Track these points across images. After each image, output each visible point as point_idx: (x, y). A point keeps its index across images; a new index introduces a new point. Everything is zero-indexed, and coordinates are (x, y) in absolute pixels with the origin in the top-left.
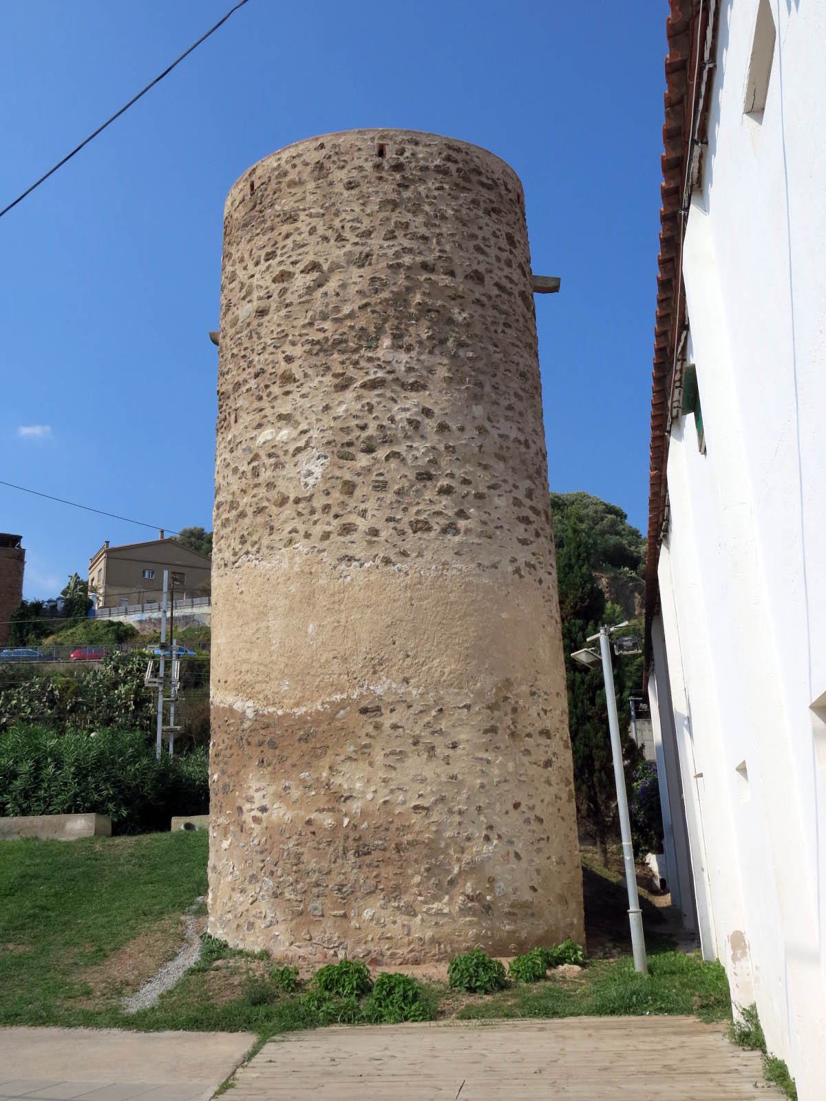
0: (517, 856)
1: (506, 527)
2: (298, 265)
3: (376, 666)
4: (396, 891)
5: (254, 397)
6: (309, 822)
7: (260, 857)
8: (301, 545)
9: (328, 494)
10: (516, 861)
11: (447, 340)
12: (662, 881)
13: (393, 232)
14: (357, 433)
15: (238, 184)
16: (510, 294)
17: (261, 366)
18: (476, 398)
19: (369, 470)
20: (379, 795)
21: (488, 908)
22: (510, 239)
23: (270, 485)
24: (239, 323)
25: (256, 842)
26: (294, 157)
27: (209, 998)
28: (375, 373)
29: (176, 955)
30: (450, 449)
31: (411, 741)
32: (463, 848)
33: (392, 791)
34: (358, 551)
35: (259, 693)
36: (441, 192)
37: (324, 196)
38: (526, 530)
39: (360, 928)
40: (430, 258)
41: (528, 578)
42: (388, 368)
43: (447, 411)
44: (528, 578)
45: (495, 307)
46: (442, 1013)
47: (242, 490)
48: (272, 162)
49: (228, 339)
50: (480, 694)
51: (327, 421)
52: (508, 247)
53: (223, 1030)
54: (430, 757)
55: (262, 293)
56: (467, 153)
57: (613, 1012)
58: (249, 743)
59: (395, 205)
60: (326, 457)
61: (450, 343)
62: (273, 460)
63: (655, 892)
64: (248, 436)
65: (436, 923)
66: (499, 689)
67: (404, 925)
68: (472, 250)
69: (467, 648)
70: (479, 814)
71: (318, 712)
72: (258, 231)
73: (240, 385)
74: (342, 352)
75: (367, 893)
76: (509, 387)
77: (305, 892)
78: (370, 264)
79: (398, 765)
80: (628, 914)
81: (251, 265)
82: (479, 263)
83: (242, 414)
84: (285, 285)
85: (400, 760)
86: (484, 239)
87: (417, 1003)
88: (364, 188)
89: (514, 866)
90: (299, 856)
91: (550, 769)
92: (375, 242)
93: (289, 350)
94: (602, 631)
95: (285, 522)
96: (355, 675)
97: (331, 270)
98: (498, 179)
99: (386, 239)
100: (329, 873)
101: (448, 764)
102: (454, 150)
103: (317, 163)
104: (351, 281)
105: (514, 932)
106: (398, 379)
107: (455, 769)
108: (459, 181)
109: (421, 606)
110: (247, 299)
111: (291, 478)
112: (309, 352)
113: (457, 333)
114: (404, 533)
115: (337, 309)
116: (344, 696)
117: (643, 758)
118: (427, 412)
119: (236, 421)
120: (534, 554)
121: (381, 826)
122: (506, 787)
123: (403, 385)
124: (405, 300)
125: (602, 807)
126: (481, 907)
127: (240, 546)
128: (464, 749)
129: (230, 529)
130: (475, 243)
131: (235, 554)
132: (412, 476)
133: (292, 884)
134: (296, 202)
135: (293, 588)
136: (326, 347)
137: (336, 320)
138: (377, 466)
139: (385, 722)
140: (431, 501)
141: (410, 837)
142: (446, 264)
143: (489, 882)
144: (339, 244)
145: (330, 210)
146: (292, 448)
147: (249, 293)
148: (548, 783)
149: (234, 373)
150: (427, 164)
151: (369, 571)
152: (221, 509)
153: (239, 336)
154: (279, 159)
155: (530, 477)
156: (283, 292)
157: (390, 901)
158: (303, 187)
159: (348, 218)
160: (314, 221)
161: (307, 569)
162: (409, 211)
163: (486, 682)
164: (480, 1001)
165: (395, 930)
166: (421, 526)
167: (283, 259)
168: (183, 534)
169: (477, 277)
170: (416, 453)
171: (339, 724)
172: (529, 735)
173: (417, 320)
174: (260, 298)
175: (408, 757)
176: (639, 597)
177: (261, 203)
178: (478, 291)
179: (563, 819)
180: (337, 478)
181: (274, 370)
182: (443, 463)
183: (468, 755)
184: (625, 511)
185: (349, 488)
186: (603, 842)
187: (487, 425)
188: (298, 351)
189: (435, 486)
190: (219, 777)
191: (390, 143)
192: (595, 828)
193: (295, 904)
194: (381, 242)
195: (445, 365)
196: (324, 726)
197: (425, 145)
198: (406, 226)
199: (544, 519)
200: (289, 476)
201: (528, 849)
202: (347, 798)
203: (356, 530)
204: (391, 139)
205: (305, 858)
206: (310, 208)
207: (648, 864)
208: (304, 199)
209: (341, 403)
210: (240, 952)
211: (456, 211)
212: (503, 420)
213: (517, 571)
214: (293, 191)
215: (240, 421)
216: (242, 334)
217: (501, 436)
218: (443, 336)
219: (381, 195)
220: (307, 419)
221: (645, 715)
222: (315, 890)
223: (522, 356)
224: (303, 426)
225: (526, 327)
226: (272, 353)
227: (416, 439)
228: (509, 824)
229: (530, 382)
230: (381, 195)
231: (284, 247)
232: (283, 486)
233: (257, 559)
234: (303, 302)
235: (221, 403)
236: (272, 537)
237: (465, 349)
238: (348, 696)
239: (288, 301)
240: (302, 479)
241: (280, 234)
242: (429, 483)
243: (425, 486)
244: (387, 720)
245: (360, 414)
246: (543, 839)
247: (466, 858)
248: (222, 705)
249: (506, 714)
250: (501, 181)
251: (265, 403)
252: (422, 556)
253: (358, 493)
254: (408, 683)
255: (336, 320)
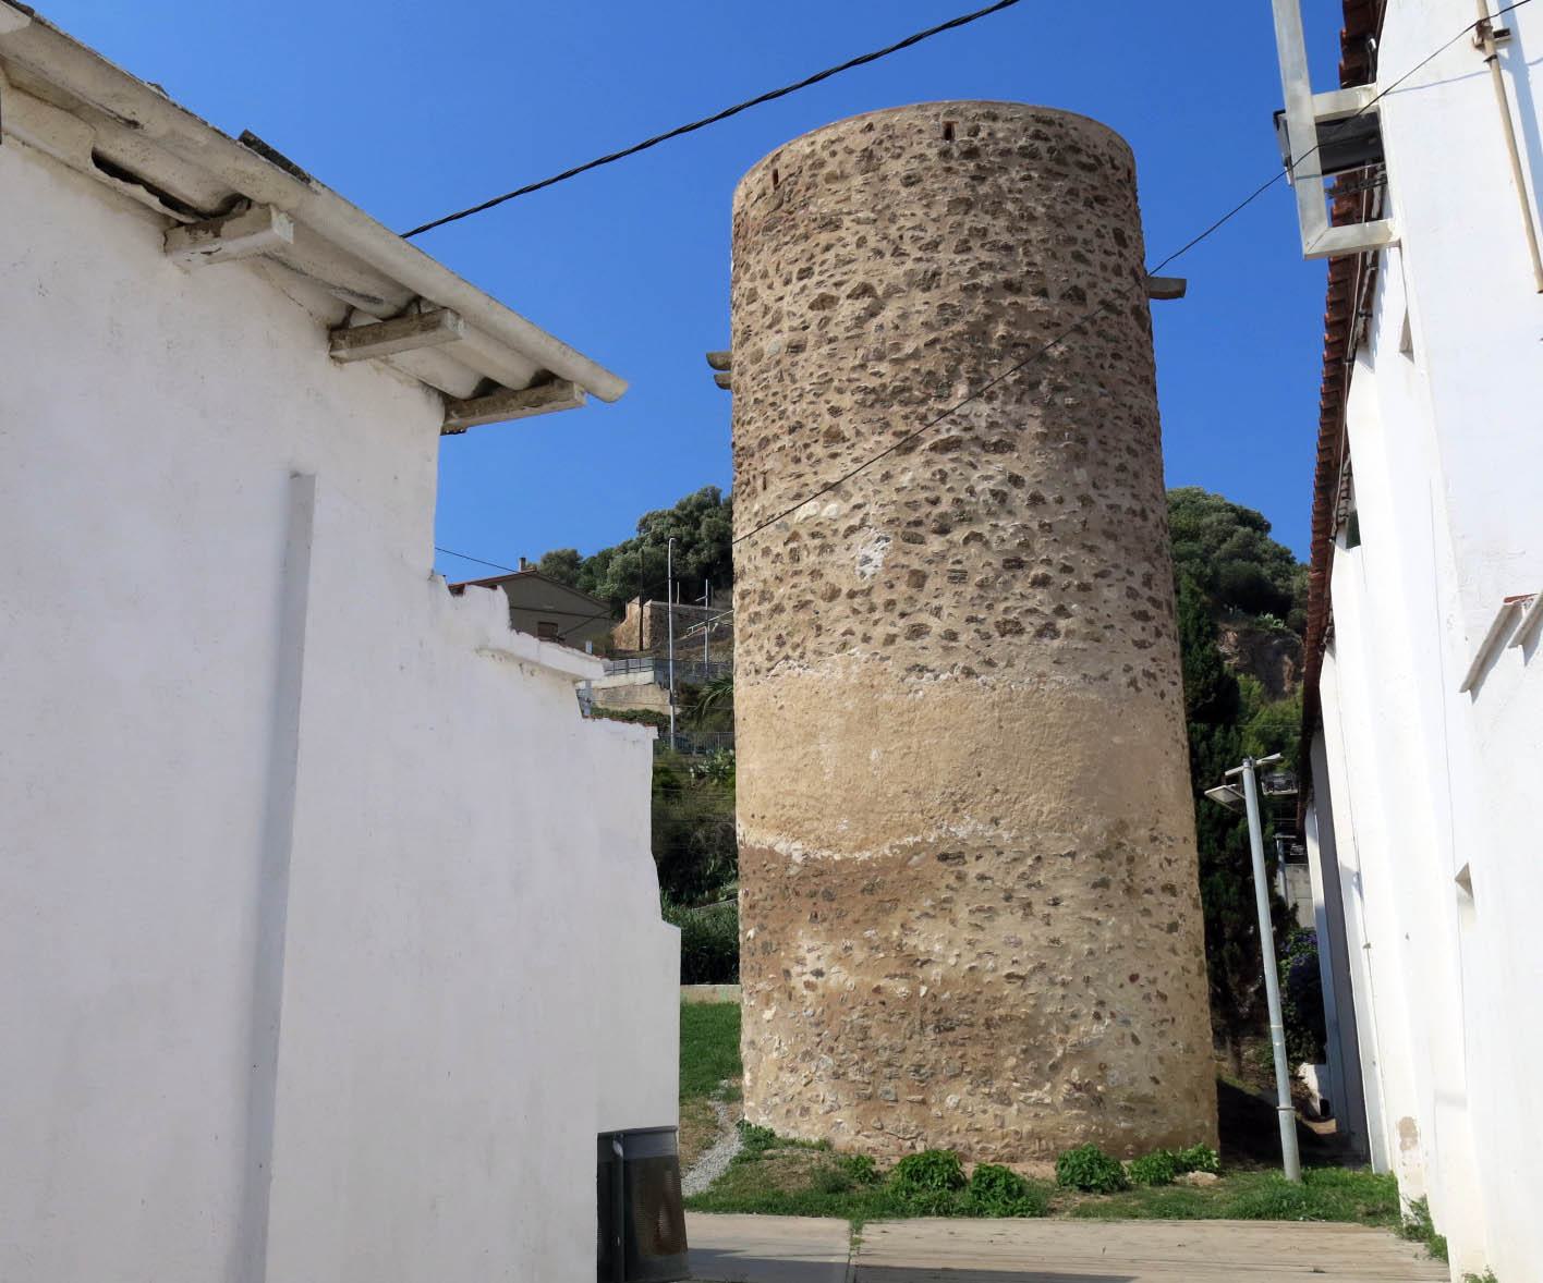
0: (1135, 1040)
1: (1119, 626)
2: (843, 288)
3: (958, 804)
4: (987, 1075)
5: (789, 459)
6: (877, 990)
7: (815, 1030)
8: (858, 651)
9: (892, 586)
10: (1133, 1046)
11: (1039, 383)
12: (1324, 1103)
13: (966, 241)
14: (926, 508)
15: (754, 172)
16: (1120, 313)
17: (798, 419)
18: (1077, 458)
19: (944, 557)
20: (963, 960)
21: (1099, 1101)
22: (1119, 237)
23: (815, 574)
24: (765, 360)
25: (810, 1011)
26: (833, 142)
27: (773, 1186)
28: (948, 430)
29: (713, 1143)
30: (1046, 528)
31: (1002, 895)
32: (1067, 1027)
33: (979, 956)
34: (932, 659)
35: (809, 832)
36: (1027, 183)
37: (876, 195)
38: (1143, 629)
39: (942, 1117)
40: (1016, 274)
41: (1146, 691)
42: (965, 424)
43: (1041, 478)
44: (1146, 691)
45: (1100, 334)
46: (1053, 1210)
47: (777, 578)
48: (802, 146)
49: (747, 378)
50: (1088, 839)
51: (888, 494)
52: (1116, 249)
53: (803, 1215)
54: (1026, 915)
55: (796, 322)
56: (1061, 125)
57: (1259, 1216)
58: (797, 894)
59: (968, 205)
60: (887, 540)
61: (1043, 388)
62: (817, 542)
63: (1316, 1119)
64: (783, 509)
65: (1036, 1115)
66: (1111, 833)
67: (996, 1116)
68: (1069, 258)
69: (1071, 782)
70: (1087, 986)
71: (885, 858)
72: (787, 239)
73: (768, 440)
74: (905, 403)
75: (951, 1077)
76: (1120, 440)
77: (874, 1072)
78: (938, 286)
79: (986, 925)
80: (1277, 1111)
81: (778, 283)
82: (1078, 276)
83: (772, 478)
84: (827, 313)
85: (989, 919)
86: (1085, 242)
87: (1024, 1198)
88: (929, 184)
89: (1132, 1052)
90: (865, 1030)
91: (1175, 934)
92: (944, 256)
93: (836, 400)
94: (1246, 764)
95: (837, 620)
96: (931, 814)
97: (888, 294)
98: (1103, 154)
99: (957, 252)
100: (903, 1051)
101: (1048, 924)
102: (1044, 122)
103: (866, 150)
104: (913, 310)
105: (1131, 1130)
106: (977, 438)
107: (1058, 930)
108: (1051, 165)
109: (1012, 729)
110: (775, 329)
111: (843, 565)
112: (862, 404)
113: (1052, 372)
114: (989, 637)
115: (897, 347)
116: (918, 839)
117: (1296, 924)
118: (1016, 481)
119: (765, 488)
120: (1154, 660)
121: (967, 996)
122: (1119, 954)
123: (984, 446)
124: (985, 333)
125: (1235, 993)
126: (1090, 1098)
127: (777, 649)
128: (1067, 906)
129: (762, 626)
130: (1073, 248)
131: (770, 658)
132: (997, 564)
133: (857, 1063)
134: (838, 202)
135: (849, 705)
136: (883, 396)
137: (895, 361)
138: (954, 551)
139: (970, 871)
140: (1022, 595)
141: (1002, 1011)
142: (1036, 282)
143: (1101, 1069)
144: (897, 260)
145: (884, 215)
146: (842, 526)
147: (776, 321)
148: (1173, 951)
149: (760, 424)
150: (1009, 146)
151: (946, 685)
152: (747, 600)
153: (765, 376)
154: (813, 143)
155: (1148, 559)
156: (825, 322)
157: (978, 1086)
158: (846, 182)
159: (909, 224)
160: (863, 230)
161: (867, 681)
162: (987, 212)
163: (1094, 825)
164: (1097, 1201)
165: (986, 1121)
166: (1010, 628)
167: (822, 278)
168: (549, 559)
169: (1076, 296)
170: (1001, 533)
171: (912, 873)
172: (1149, 891)
173: (1001, 358)
174: (793, 329)
175: (998, 915)
176: (1290, 662)
177: (789, 201)
178: (1079, 313)
179: (1192, 997)
180: (903, 567)
181: (815, 425)
182: (1037, 546)
183: (1073, 914)
184: (1267, 518)
185: (918, 579)
186: (1235, 1043)
187: (1092, 493)
188: (846, 401)
189: (1027, 576)
190: (756, 933)
191: (960, 120)
192: (1224, 1022)
193: (861, 1086)
194: (953, 256)
195: (1037, 417)
196: (894, 875)
197: (1006, 120)
198: (984, 232)
199: (1166, 612)
200: (840, 562)
201: (1146, 1029)
202: (925, 963)
203: (928, 633)
204: (961, 115)
205: (873, 1033)
206: (857, 212)
207: (1302, 1078)
208: (848, 199)
209: (904, 470)
210: (793, 1142)
211: (1048, 207)
212: (1112, 486)
213: (1133, 683)
214: (834, 187)
215: (771, 488)
216: (769, 374)
217: (1111, 507)
218: (1033, 378)
219: (950, 192)
220: (861, 489)
221: (1302, 860)
222: (887, 1071)
223: (1136, 397)
224: (857, 499)
225: (1140, 354)
226: (812, 403)
227: (1003, 516)
228: (1126, 999)
229: (1147, 429)
230: (950, 192)
231: (823, 263)
232: (831, 575)
233: (800, 666)
234: (851, 337)
235: (740, 460)
236: (820, 639)
237: (1062, 394)
238: (923, 840)
239: (831, 335)
240: (857, 567)
241: (817, 245)
242: (1019, 573)
243: (1013, 576)
244: (973, 869)
245: (931, 484)
246: (1167, 1020)
247: (1072, 1038)
248: (758, 846)
249: (1120, 865)
250: (1107, 158)
251: (804, 467)
252: (1012, 666)
253: (930, 585)
254: (997, 824)
255: (895, 361)
